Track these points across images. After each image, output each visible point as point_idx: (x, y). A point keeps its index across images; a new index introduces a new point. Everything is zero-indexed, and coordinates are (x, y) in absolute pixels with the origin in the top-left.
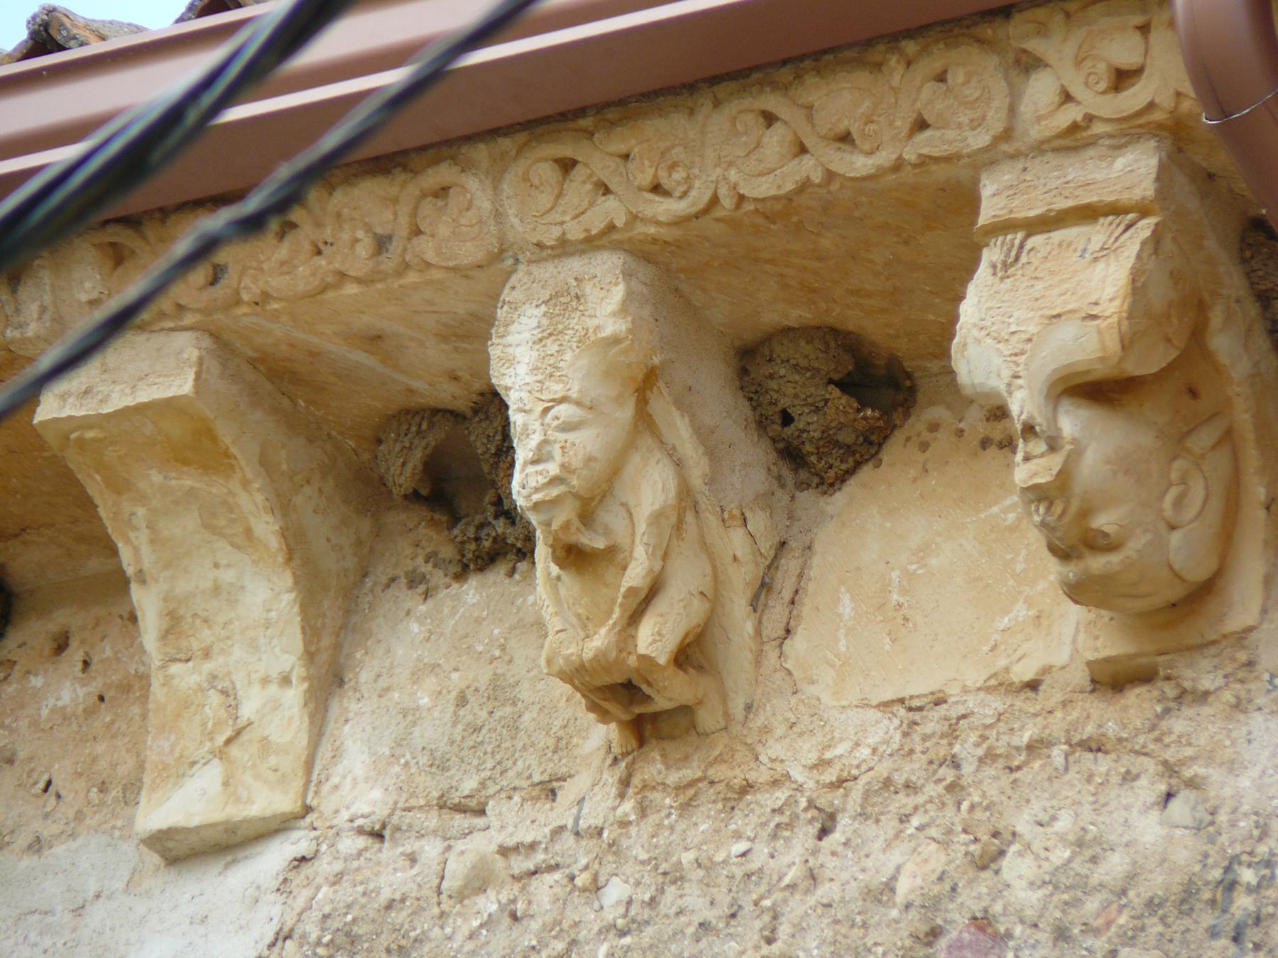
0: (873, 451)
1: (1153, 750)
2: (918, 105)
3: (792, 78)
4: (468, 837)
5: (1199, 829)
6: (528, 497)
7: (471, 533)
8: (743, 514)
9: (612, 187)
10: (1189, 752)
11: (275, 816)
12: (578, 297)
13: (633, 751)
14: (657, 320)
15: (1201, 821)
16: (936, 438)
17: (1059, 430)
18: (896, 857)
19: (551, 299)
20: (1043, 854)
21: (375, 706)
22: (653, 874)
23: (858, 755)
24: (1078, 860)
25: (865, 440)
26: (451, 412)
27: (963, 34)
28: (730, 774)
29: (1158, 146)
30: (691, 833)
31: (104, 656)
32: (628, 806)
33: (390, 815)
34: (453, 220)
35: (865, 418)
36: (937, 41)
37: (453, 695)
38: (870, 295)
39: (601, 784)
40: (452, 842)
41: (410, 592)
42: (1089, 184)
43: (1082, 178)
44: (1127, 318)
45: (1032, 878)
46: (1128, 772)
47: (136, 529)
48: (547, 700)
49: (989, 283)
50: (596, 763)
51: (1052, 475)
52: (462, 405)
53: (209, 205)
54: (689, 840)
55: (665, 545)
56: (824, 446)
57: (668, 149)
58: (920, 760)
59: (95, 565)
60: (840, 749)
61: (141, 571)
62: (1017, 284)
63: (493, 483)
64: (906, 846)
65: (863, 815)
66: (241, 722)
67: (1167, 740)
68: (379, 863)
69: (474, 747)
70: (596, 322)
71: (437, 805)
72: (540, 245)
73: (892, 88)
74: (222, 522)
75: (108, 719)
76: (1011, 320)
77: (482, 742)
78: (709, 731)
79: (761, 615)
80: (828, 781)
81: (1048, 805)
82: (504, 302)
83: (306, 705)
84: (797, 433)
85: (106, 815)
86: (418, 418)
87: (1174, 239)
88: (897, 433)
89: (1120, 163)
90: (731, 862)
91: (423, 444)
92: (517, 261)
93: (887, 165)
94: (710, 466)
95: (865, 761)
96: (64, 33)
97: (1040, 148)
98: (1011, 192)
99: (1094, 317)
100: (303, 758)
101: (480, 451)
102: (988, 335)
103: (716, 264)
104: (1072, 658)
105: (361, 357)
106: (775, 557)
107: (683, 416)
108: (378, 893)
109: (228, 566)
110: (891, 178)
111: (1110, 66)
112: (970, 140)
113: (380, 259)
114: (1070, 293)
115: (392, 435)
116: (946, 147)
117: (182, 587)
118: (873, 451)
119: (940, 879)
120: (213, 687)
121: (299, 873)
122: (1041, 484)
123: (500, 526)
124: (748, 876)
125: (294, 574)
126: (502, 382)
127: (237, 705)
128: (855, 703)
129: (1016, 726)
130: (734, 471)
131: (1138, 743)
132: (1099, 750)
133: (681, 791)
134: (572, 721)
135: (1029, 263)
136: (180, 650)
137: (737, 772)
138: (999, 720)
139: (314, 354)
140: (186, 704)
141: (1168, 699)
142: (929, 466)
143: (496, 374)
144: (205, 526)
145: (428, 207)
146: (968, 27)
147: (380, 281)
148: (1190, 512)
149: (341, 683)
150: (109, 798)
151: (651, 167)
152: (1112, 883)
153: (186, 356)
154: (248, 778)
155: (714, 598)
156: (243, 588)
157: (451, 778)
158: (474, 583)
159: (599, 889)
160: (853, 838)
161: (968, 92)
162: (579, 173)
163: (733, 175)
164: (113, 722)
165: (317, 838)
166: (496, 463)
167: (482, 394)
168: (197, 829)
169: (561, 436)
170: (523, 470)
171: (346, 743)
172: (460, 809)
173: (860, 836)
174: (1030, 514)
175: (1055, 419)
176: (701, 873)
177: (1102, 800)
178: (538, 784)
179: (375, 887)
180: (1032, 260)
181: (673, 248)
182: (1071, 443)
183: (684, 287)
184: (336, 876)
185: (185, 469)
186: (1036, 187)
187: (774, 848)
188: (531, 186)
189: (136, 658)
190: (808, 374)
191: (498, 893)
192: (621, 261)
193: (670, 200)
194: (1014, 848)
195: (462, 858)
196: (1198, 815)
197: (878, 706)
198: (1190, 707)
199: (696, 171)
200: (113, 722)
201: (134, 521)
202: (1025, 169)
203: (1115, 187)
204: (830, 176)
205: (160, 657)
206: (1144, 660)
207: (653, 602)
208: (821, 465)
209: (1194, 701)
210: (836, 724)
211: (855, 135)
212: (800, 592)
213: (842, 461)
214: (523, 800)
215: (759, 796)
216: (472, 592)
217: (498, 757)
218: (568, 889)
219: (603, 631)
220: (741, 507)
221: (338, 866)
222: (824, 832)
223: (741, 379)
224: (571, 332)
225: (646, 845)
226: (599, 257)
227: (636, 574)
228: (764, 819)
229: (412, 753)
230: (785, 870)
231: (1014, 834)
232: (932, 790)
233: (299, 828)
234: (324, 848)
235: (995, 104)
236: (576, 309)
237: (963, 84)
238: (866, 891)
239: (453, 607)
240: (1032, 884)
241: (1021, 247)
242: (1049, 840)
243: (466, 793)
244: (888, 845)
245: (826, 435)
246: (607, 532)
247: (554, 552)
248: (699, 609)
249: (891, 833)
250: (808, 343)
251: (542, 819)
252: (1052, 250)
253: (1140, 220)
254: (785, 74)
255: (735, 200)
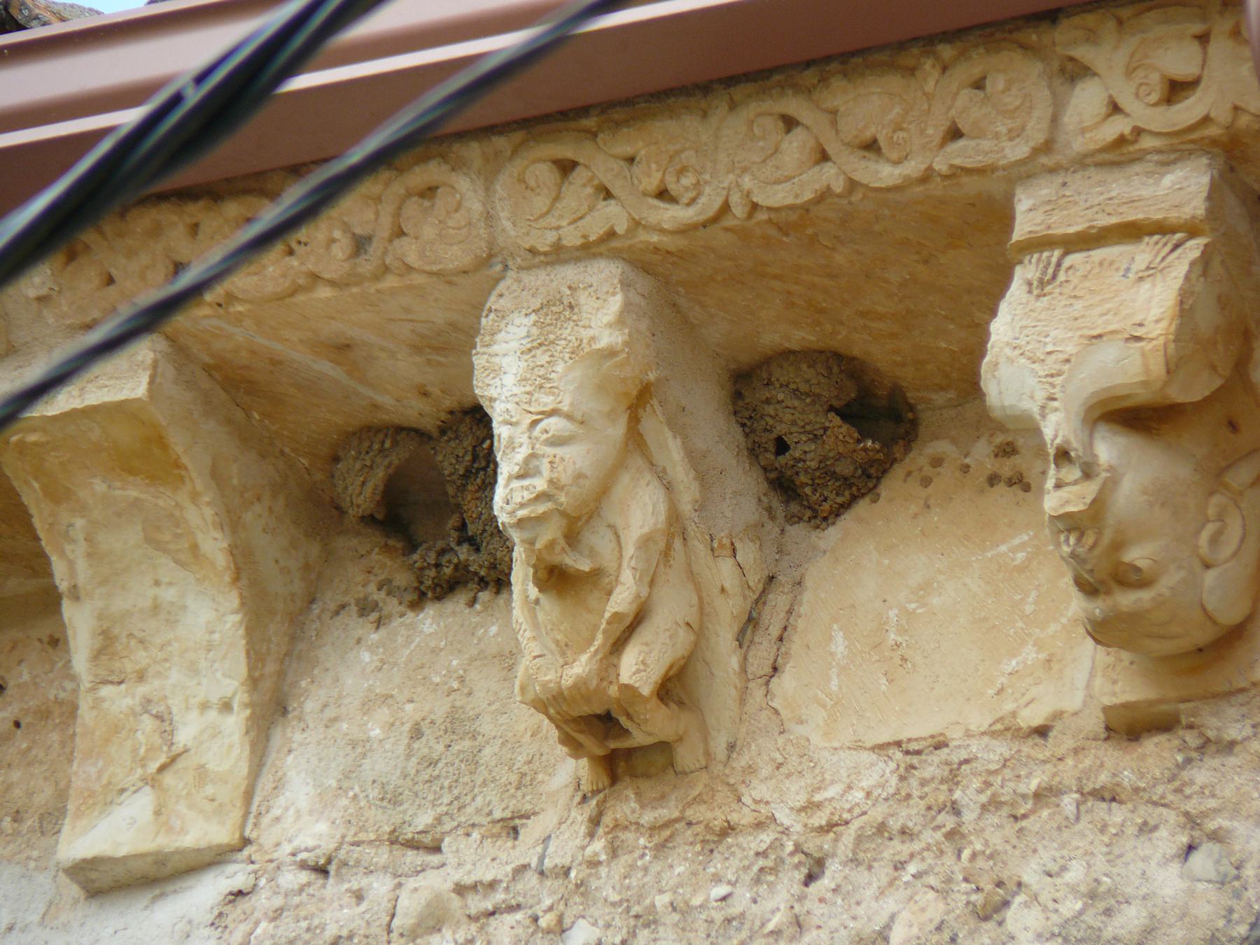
0: (871, 485)
1: (1172, 802)
2: (953, 112)
3: (816, 81)
4: (421, 875)
5: (1223, 883)
6: (512, 513)
7: (432, 559)
8: (732, 544)
9: (614, 191)
10: (1212, 803)
11: (210, 848)
12: (571, 307)
13: (604, 789)
14: (654, 335)
15: (1226, 875)
16: (939, 474)
17: (1095, 456)
18: (890, 904)
19: (542, 308)
20: (1051, 905)
21: (322, 736)
22: (624, 916)
23: (850, 798)
24: (1091, 912)
25: (864, 472)
26: (416, 431)
27: (1005, 39)
28: (709, 815)
29: (1210, 165)
30: (666, 875)
31: (21, 681)
32: (598, 846)
33: (337, 849)
34: (440, 222)
35: (865, 450)
36: (976, 46)
37: (407, 727)
38: (881, 317)
39: (569, 822)
40: (403, 880)
41: (361, 620)
42: (1134, 201)
43: (1126, 195)
44: (1174, 341)
45: (1040, 930)
46: (1145, 823)
47: (73, 541)
48: (510, 734)
49: (1024, 301)
50: (563, 800)
51: (1085, 504)
52: (429, 424)
53: (173, 199)
54: (664, 883)
55: (653, 569)
56: (819, 477)
57: (678, 152)
58: (917, 806)
59: (16, 585)
60: (830, 793)
61: (75, 587)
62: (1053, 302)
63: (458, 506)
64: (902, 894)
65: (854, 861)
66: (176, 749)
67: (1188, 791)
68: (322, 900)
69: (430, 781)
70: (591, 333)
71: (388, 840)
72: (532, 251)
73: (925, 93)
74: (167, 537)
75: (24, 746)
76: (1047, 340)
77: (438, 776)
78: (687, 770)
79: (747, 651)
80: (817, 825)
81: (1057, 854)
82: (490, 310)
83: (247, 732)
84: (792, 463)
85: (20, 845)
86: (381, 436)
87: (1223, 262)
88: (896, 466)
89: (1168, 180)
90: (710, 906)
91: (386, 462)
92: (506, 267)
93: (915, 175)
94: (701, 492)
95: (858, 804)
96: (26, 13)
97: (1083, 162)
98: (1049, 207)
99: (1138, 339)
100: (243, 788)
101: (446, 472)
102: (1022, 354)
103: (719, 278)
104: (1085, 704)
105: (325, 367)
106: (764, 591)
107: (675, 437)
108: (323, 930)
109: (170, 584)
110: (919, 189)
111: (1163, 76)
112: (1007, 151)
113: (357, 261)
114: (537, 757)
115: (353, 453)
116: (980, 158)
117: (120, 604)
118: (871, 485)
119: (939, 929)
120: (146, 712)
121: (235, 907)
122: (1073, 513)
123: (464, 553)
124: (729, 921)
125: (241, 594)
126: (486, 393)
127: (173, 731)
128: (848, 744)
129: (1022, 773)
130: (724, 499)
131: (1156, 793)
132: (1113, 799)
133: (656, 832)
134: (537, 757)
135: (1067, 281)
136: (112, 672)
137: (718, 813)
138: (1004, 766)
139: (276, 362)
140: (116, 729)
141: (1190, 749)
142: (931, 502)
143: (480, 384)
144: (149, 540)
145: (413, 208)
146: (1011, 32)
147: (356, 284)
148: (1227, 551)
149: (284, 711)
150: (24, 827)
151: (658, 171)
152: (1128, 937)
153: (140, 358)
154: (182, 808)
155: (699, 630)
156: (184, 607)
157: (405, 812)
158: (431, 612)
159: (563, 931)
160: (843, 884)
161: (1007, 100)
162: (579, 175)
163: (747, 182)
164: (29, 749)
165: (256, 872)
166: (464, 486)
167: (451, 413)
168: (125, 859)
169: (550, 451)
170: (507, 486)
171: (289, 774)
172: (412, 845)
173: (850, 883)
174: (1058, 545)
175: (1091, 445)
176: (676, 917)
177: (1117, 851)
178: (499, 821)
179: (320, 923)
180: (1071, 278)
181: (675, 259)
182: (1107, 471)
183: (682, 302)
184: (276, 911)
185: (131, 479)
186: (1076, 203)
187: (757, 893)
188: (527, 188)
189: (57, 683)
190: (808, 400)
191: (454, 933)
192: (620, 270)
193: (676, 207)
194: (1019, 899)
195: (415, 895)
196: (1222, 869)
197: (873, 749)
198: (1213, 758)
199: (707, 177)
200: (29, 749)
201: (72, 533)
202: (1064, 184)
203: (1163, 205)
204: (853, 185)
205: (91, 678)
206: (1164, 707)
207: (639, 630)
208: (814, 498)
209: (1218, 751)
210: (827, 766)
211: (882, 143)
212: (789, 629)
213: (837, 494)
214: (483, 837)
215: (741, 839)
216: (429, 621)
217: (456, 792)
218: (531, 930)
219: (584, 658)
220: (730, 536)
221: (278, 902)
222: (810, 879)
223: (734, 403)
224: (563, 342)
225: (618, 887)
226: (596, 265)
227: (622, 599)
228: (746, 863)
229: (361, 786)
230: (768, 916)
231: (1019, 884)
232: (929, 837)
233: (235, 862)
234: (263, 882)
235: (1036, 113)
236: (569, 319)
237: (1003, 92)
238: (858, 939)
239: (408, 637)
240: (1039, 936)
241: (1059, 265)
242: (1058, 891)
243: (420, 828)
244: (882, 893)
245: (822, 465)
246: (592, 554)
247: (535, 573)
248: (684, 640)
249: (885, 880)
250: (809, 367)
251: (503, 857)
252: (1092, 268)
253: (1187, 240)
254: (810, 76)
255: (747, 209)
